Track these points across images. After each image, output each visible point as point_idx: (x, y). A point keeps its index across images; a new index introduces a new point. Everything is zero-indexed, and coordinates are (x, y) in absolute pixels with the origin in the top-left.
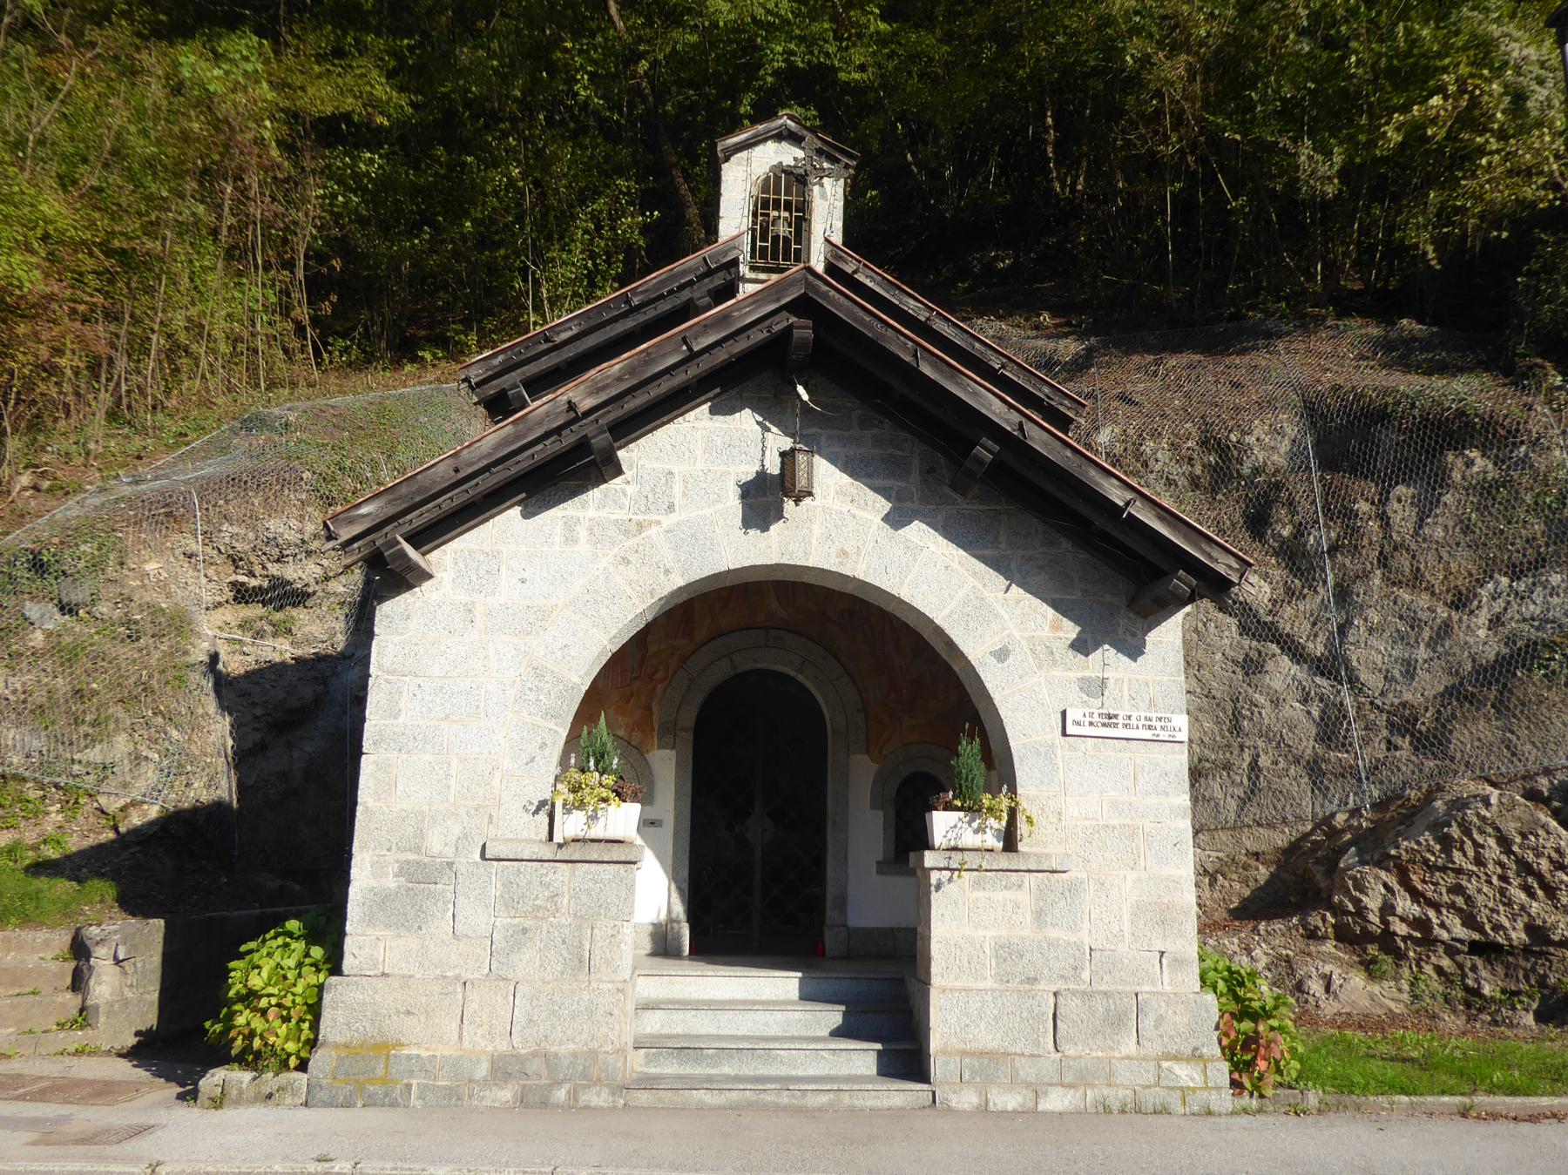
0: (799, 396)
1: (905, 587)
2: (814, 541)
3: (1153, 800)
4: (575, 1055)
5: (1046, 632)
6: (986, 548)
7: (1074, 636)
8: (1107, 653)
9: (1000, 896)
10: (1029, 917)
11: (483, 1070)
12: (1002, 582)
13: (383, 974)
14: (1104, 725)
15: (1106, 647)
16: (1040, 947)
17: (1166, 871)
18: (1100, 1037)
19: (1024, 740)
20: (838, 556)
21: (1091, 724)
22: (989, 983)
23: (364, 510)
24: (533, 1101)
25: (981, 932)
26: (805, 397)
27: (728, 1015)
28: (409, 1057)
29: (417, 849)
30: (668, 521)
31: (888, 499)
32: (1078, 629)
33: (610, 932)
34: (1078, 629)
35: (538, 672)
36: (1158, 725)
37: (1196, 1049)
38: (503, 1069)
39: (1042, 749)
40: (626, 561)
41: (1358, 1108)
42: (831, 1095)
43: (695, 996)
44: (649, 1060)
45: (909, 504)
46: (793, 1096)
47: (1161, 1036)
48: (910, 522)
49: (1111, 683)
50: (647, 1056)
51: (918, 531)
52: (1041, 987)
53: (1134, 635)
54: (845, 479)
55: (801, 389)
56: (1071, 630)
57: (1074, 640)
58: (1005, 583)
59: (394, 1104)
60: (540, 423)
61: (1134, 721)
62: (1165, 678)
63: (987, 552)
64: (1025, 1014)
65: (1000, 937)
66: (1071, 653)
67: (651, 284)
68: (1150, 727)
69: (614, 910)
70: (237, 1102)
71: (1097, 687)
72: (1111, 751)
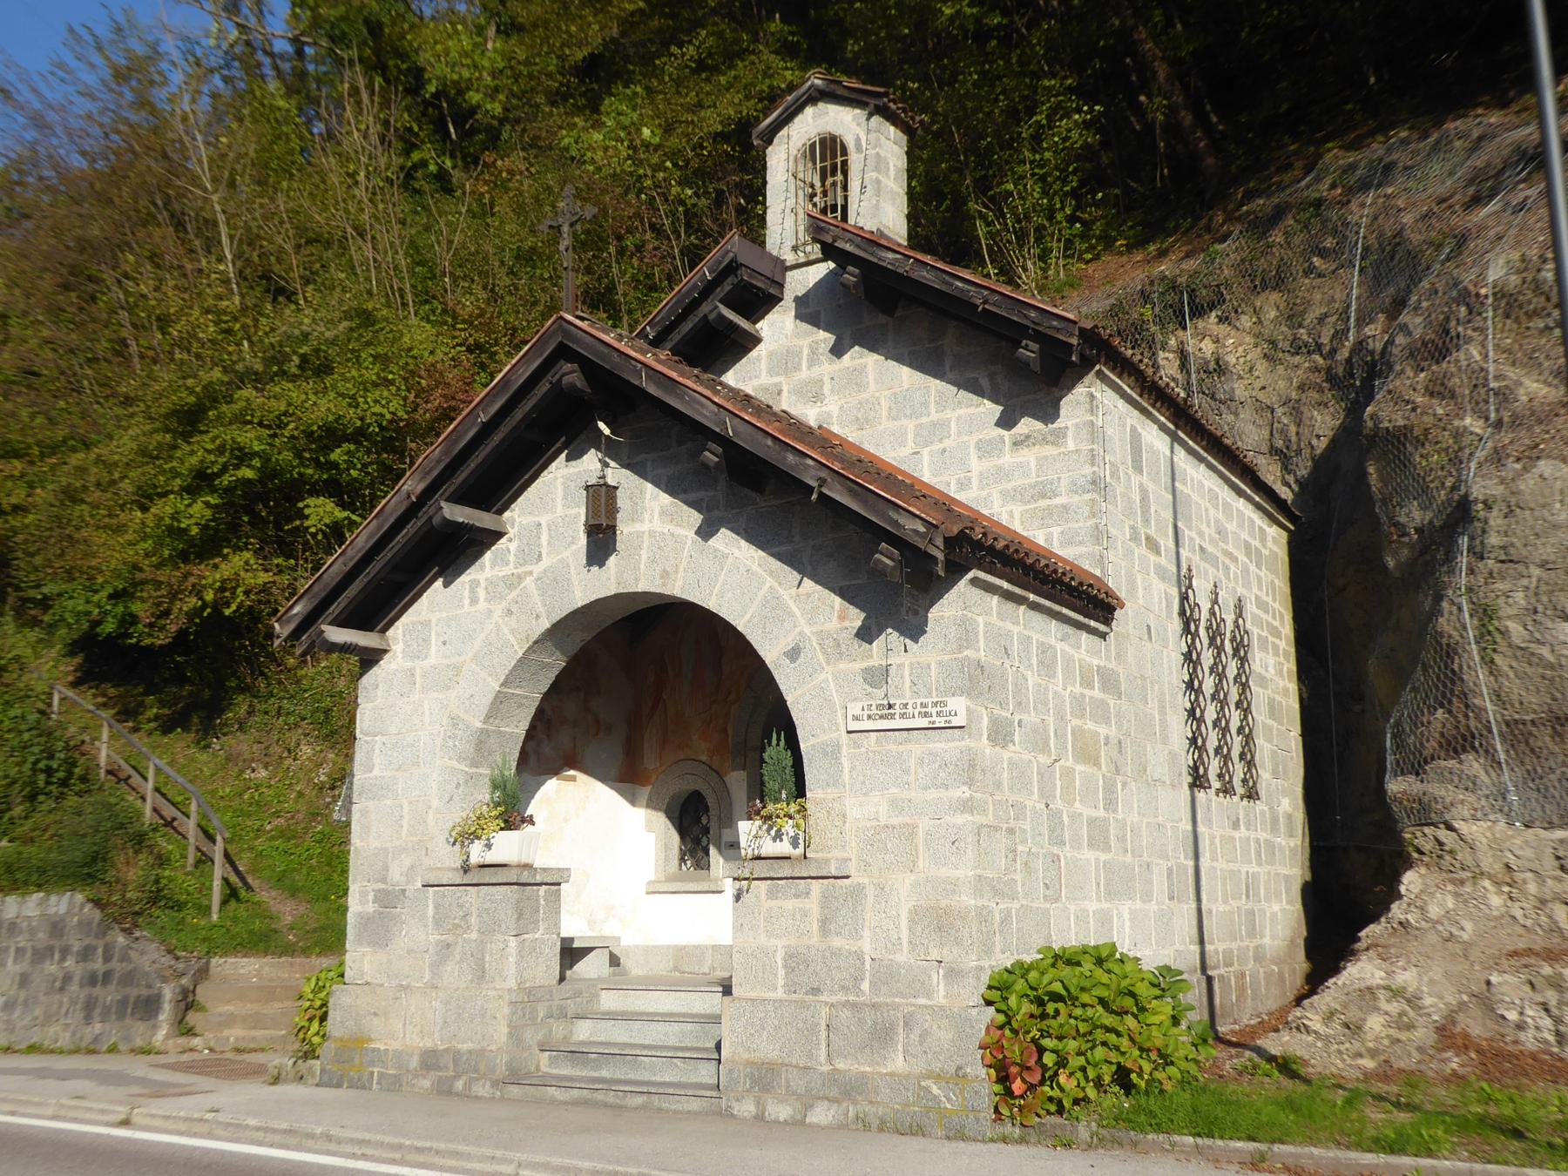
0: (601, 432)
1: (714, 598)
2: (642, 566)
3: (933, 794)
4: (470, 1052)
5: (834, 624)
6: (781, 544)
7: (859, 623)
8: (892, 637)
9: (790, 904)
10: (815, 927)
11: (414, 1063)
12: (795, 576)
13: (367, 984)
14: (881, 717)
15: (890, 630)
16: (824, 957)
17: (945, 872)
18: (868, 1050)
19: (812, 741)
20: (662, 577)
21: (869, 717)
22: (780, 994)
23: (295, 611)
24: (444, 1090)
25: (773, 941)
26: (607, 431)
27: (637, 1025)
28: (374, 1050)
29: (384, 880)
30: (537, 569)
31: (699, 511)
32: (863, 615)
33: (501, 946)
34: (863, 615)
35: (454, 721)
36: (934, 711)
37: (959, 1068)
38: (430, 1060)
39: (829, 749)
40: (510, 612)
41: (1135, 1144)
42: (645, 1097)
43: (643, 1009)
44: (552, 1061)
45: (716, 512)
46: (617, 1097)
47: (925, 1052)
48: (718, 531)
49: (892, 671)
50: (550, 1057)
51: (726, 541)
52: (822, 998)
53: (916, 613)
54: (665, 499)
55: (601, 425)
56: (856, 618)
57: (860, 629)
58: (796, 576)
59: (363, 1088)
60: (391, 514)
61: (910, 710)
62: (947, 657)
63: (783, 548)
64: (800, 1025)
65: (789, 946)
66: (856, 642)
67: (664, 311)
68: (926, 715)
69: (504, 926)
70: (286, 1081)
71: (878, 677)
72: (892, 745)
